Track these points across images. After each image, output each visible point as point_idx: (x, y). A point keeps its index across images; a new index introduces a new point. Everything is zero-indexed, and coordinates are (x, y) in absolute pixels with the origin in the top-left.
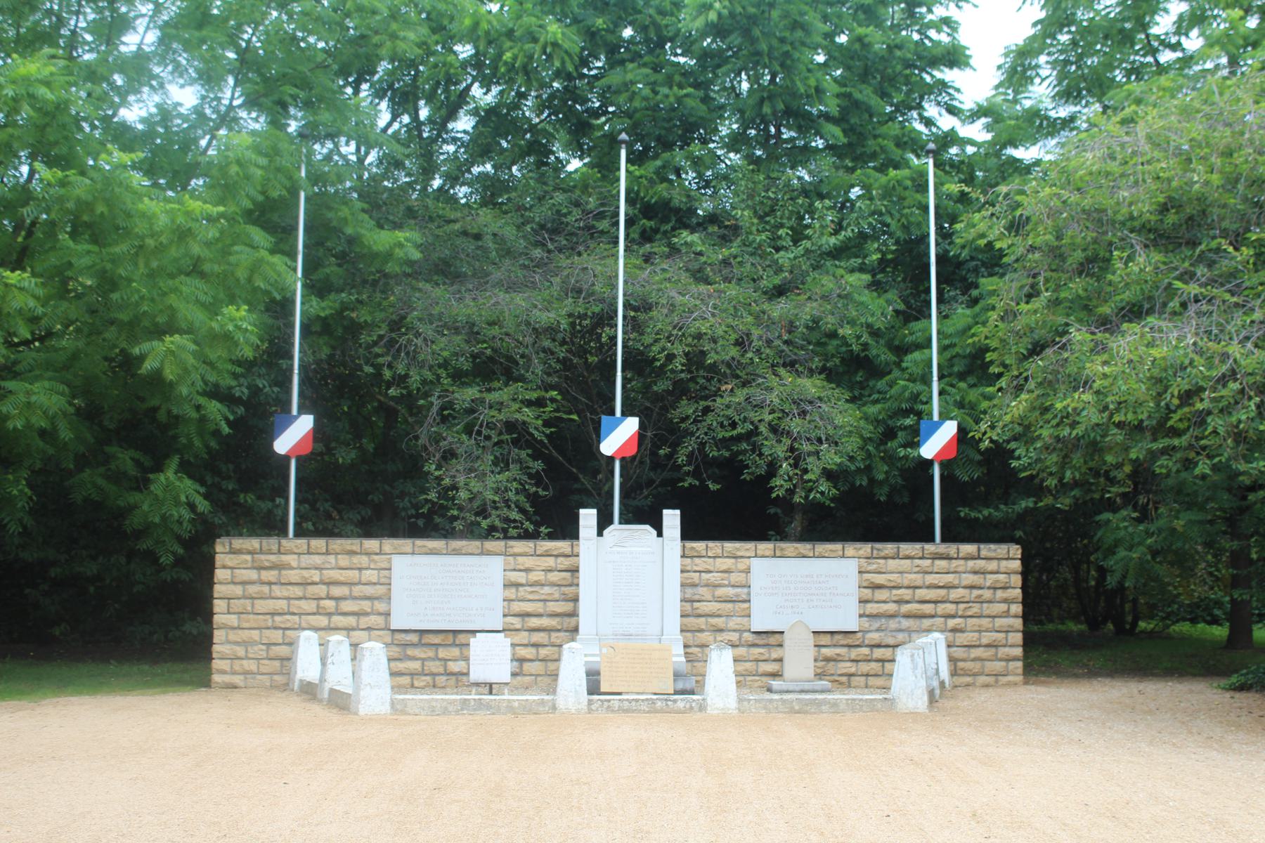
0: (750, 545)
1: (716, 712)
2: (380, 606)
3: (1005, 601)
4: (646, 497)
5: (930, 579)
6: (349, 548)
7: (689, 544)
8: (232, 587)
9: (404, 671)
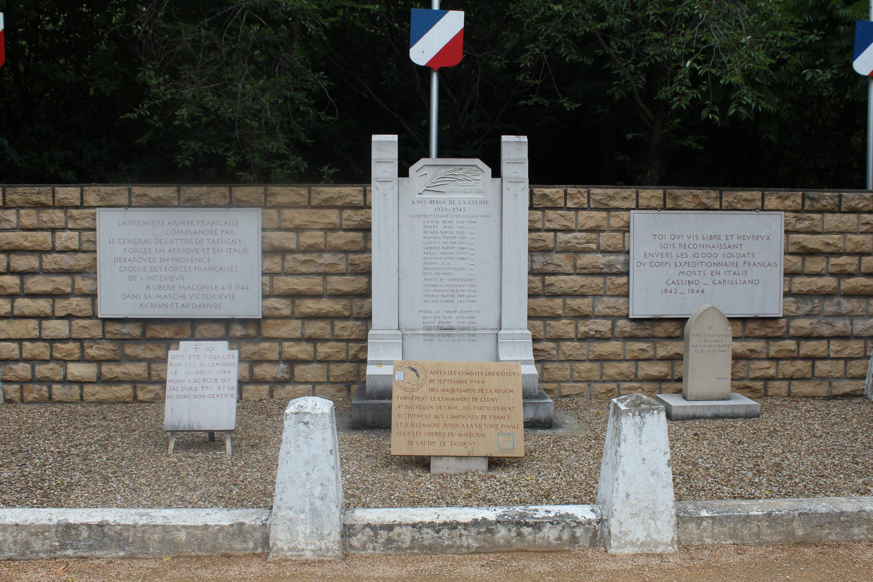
0: (629, 192)
1: (629, 550)
2: (83, 284)
6: (35, 198)
7: (538, 191)
9: (122, 377)
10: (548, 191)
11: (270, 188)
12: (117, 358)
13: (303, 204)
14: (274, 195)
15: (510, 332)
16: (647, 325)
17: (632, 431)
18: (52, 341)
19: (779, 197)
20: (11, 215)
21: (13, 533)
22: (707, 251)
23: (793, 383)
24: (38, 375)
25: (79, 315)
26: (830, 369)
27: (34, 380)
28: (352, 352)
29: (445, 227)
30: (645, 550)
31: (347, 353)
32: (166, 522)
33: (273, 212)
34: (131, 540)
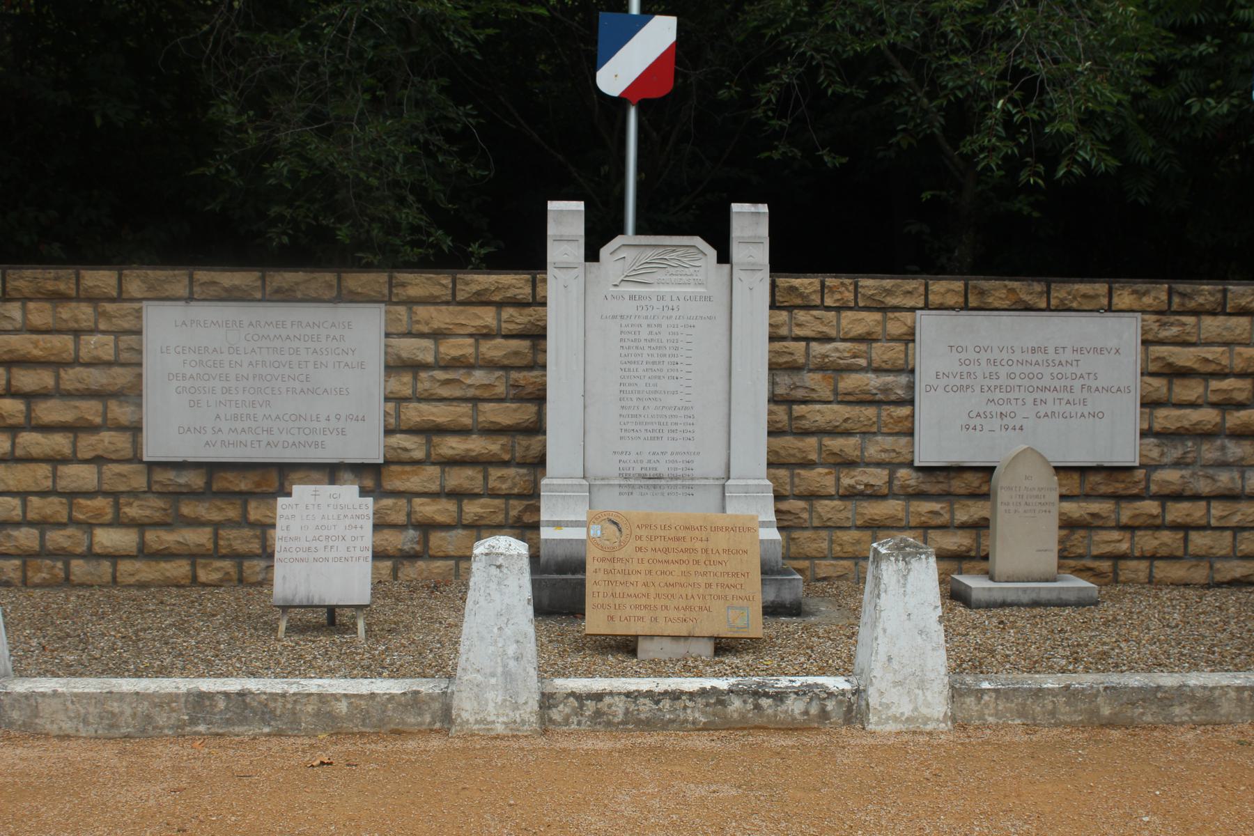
1: (892, 727)
2: (120, 412)
6: (50, 286)
7: (783, 282)
10: (796, 282)
11: (396, 275)
12: (169, 520)
13: (444, 299)
14: (403, 285)
15: (742, 482)
17: (894, 579)
19: (1134, 292)
20: (14, 310)
21: (131, 703)
22: (1027, 369)
23: (1156, 563)
24: (50, 545)
25: (113, 457)
26: (1211, 544)
28: (514, 513)
29: (651, 333)
30: (912, 727)
31: (507, 514)
32: (321, 690)
33: (402, 310)
34: (278, 712)
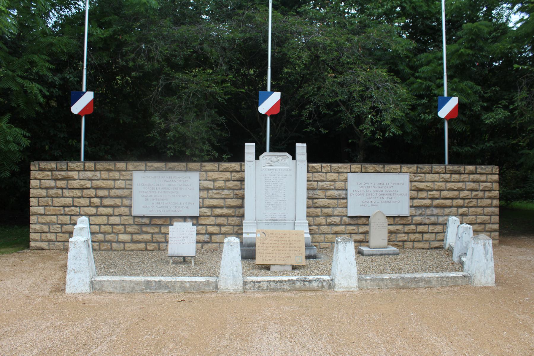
0: (347, 165)
1: (342, 290)
2: (126, 202)
3: (490, 198)
4: (284, 145)
5: (450, 185)
6: (107, 167)
7: (311, 165)
8: (40, 190)
9: (141, 240)
14: (205, 166)
16: (355, 219)
18: (113, 225)
19: (407, 168)
22: (379, 189)
24: (107, 239)
27: (105, 241)
28: (235, 230)
33: (204, 173)
